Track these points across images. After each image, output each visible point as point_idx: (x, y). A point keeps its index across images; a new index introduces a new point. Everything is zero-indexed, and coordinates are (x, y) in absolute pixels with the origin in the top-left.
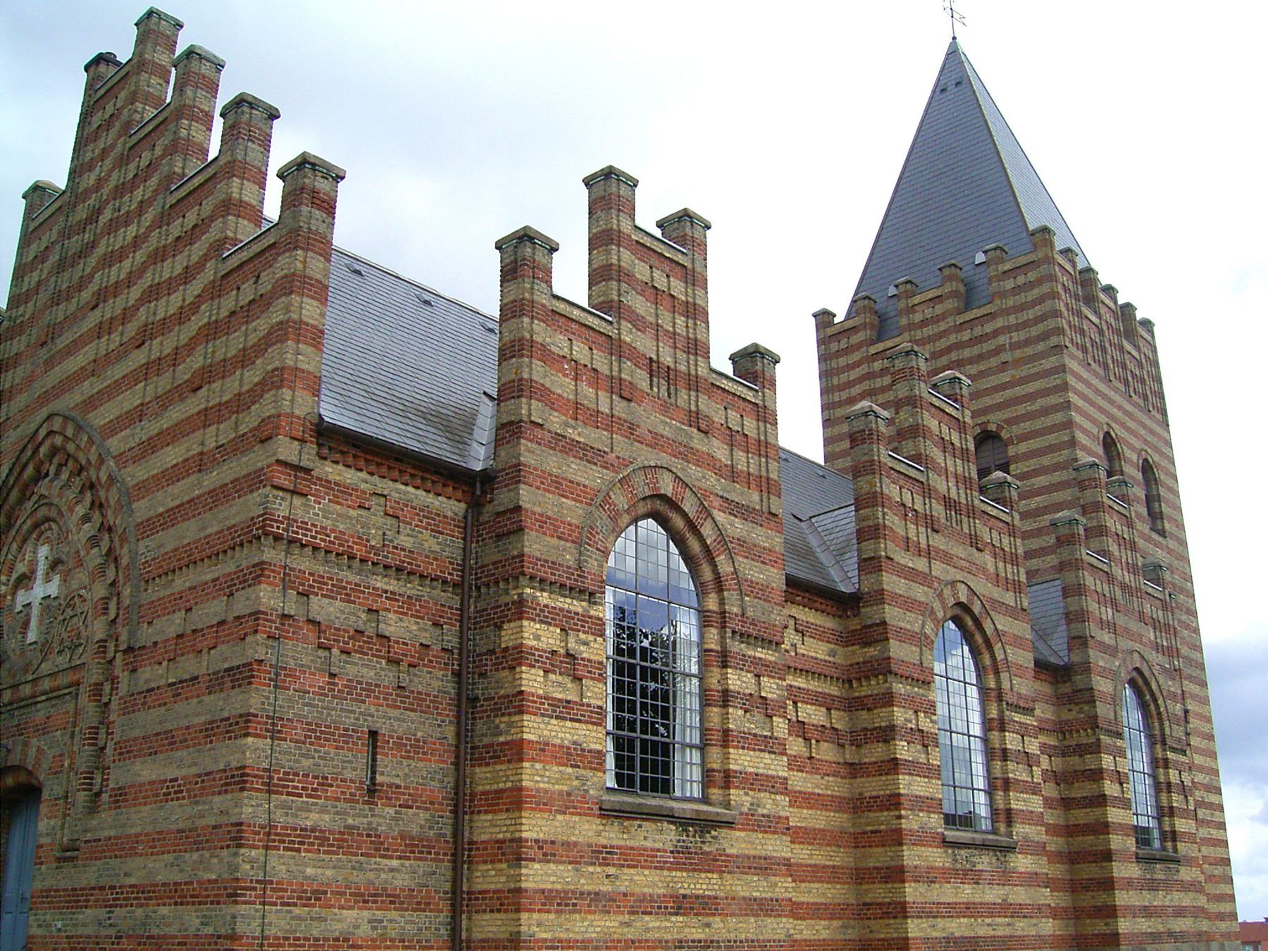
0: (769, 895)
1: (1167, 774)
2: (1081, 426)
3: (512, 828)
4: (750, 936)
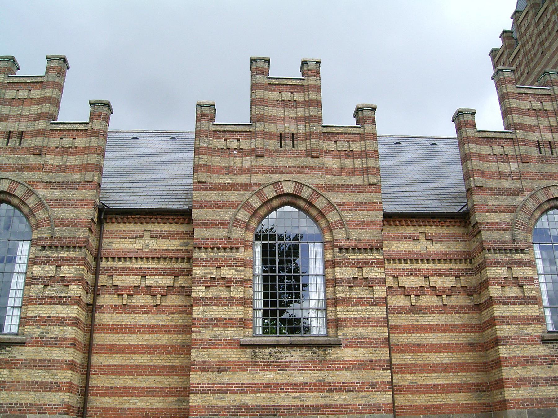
3: (441, 359)
4: (29, 402)
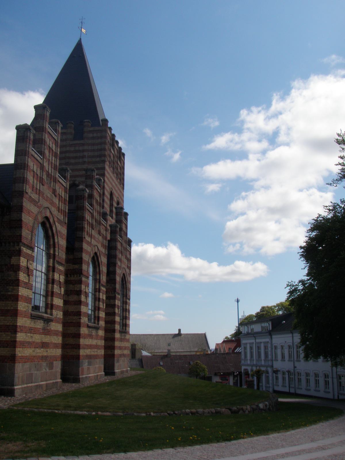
0: (57, 342)
1: (53, 275)
2: (107, 171)
